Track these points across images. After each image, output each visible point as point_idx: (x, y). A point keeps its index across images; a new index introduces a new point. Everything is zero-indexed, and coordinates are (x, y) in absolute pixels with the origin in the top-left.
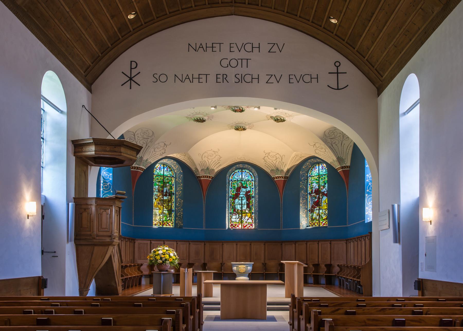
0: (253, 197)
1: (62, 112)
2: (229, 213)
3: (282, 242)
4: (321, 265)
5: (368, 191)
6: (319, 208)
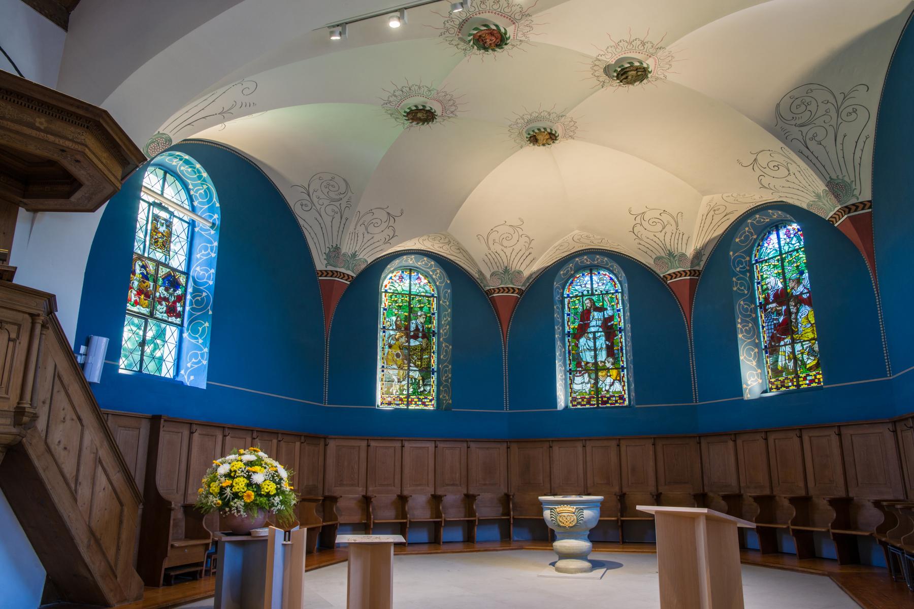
0: (620, 330)
4: (815, 499)
6: (792, 339)
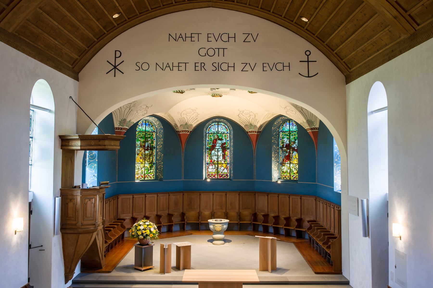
0: (228, 149)
1: (50, 111)
2: (206, 164)
3: (255, 193)
4: (291, 218)
5: (336, 160)
